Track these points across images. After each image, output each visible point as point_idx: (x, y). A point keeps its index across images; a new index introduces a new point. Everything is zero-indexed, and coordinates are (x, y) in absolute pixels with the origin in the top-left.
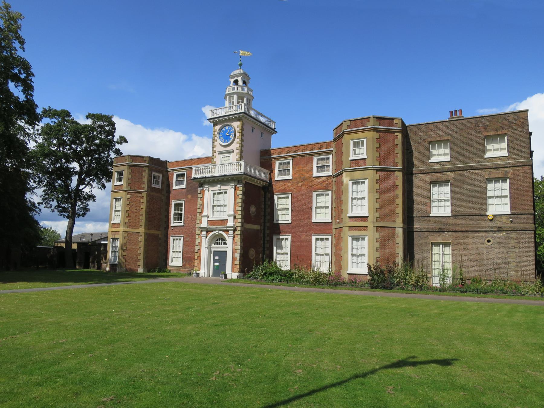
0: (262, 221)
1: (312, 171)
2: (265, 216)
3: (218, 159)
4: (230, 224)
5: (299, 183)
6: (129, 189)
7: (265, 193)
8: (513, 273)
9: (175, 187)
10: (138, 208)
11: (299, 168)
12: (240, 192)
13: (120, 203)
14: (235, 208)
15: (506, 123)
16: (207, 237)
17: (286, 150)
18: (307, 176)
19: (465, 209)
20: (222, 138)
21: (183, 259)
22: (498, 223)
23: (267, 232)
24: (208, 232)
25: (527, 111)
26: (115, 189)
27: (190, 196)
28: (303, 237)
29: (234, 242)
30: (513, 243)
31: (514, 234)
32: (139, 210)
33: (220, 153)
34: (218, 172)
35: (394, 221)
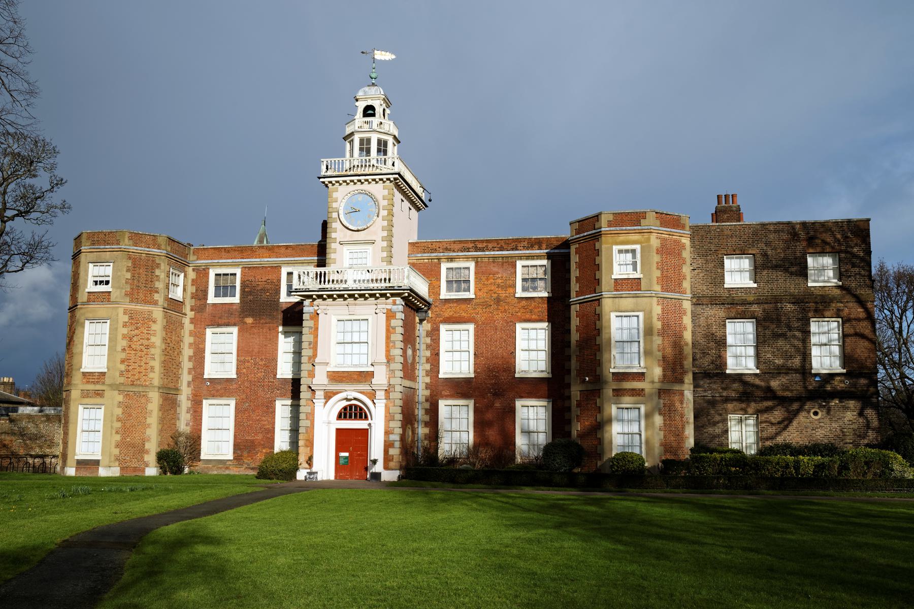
1: (514, 286)
4: (381, 378)
6: (166, 306)
9: (212, 299)
10: (145, 342)
11: (487, 279)
14: (388, 351)
17: (460, 246)
18: (503, 294)
21: (237, 446)
24: (328, 396)
25: (869, 220)
27: (249, 320)
32: (147, 347)
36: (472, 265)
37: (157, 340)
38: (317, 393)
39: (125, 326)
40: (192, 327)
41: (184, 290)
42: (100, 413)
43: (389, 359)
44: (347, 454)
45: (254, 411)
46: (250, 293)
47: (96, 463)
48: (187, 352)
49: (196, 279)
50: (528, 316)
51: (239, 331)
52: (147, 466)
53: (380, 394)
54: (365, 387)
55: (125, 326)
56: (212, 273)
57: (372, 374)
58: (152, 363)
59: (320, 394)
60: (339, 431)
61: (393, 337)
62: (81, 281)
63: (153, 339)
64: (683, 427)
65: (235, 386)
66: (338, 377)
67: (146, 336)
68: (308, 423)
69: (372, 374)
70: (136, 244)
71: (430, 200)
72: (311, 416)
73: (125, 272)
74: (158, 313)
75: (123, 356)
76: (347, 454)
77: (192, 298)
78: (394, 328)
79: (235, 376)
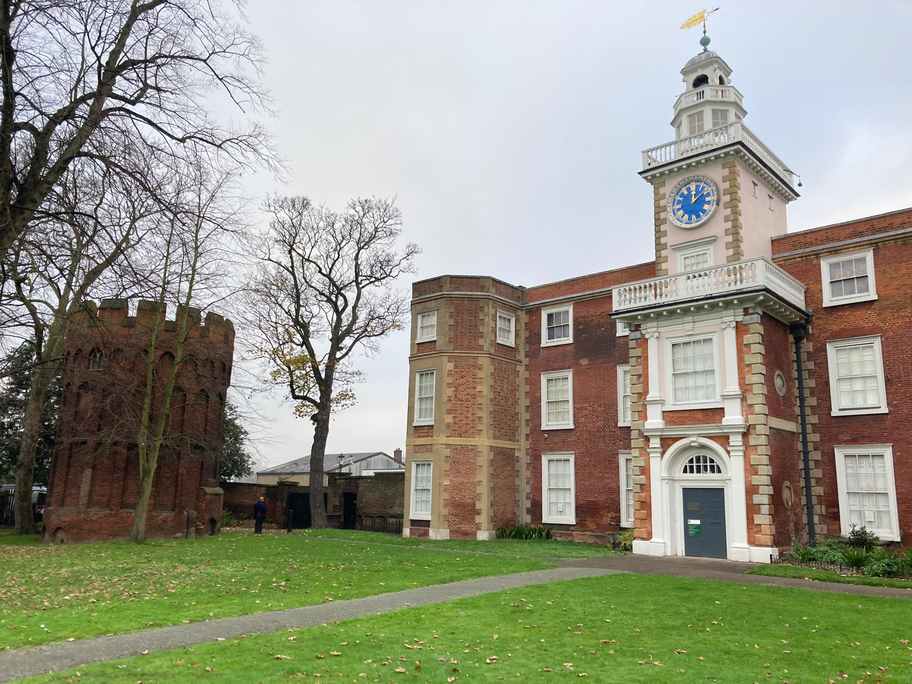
0: (797, 411)
2: (802, 399)
3: (676, 263)
4: (734, 417)
7: (798, 340)
9: (545, 342)
11: (897, 270)
12: (754, 338)
13: (432, 381)
14: (742, 378)
16: (663, 453)
21: (578, 508)
23: (814, 437)
24: (666, 442)
26: (419, 351)
27: (584, 362)
29: (751, 469)
32: (474, 397)
33: (677, 248)
34: (682, 290)
36: (869, 255)
38: (652, 441)
39: (450, 375)
40: (527, 374)
41: (517, 335)
43: (746, 389)
44: (698, 522)
45: (595, 466)
47: (427, 523)
48: (524, 402)
51: (574, 375)
52: (479, 529)
53: (736, 440)
55: (450, 375)
57: (719, 412)
58: (480, 414)
60: (688, 493)
61: (748, 359)
63: (479, 388)
65: (573, 438)
66: (672, 417)
67: (472, 385)
69: (719, 412)
70: (457, 289)
71: (800, 185)
73: (447, 319)
75: (449, 406)
76: (698, 522)
77: (526, 343)
78: (748, 346)
79: (572, 427)
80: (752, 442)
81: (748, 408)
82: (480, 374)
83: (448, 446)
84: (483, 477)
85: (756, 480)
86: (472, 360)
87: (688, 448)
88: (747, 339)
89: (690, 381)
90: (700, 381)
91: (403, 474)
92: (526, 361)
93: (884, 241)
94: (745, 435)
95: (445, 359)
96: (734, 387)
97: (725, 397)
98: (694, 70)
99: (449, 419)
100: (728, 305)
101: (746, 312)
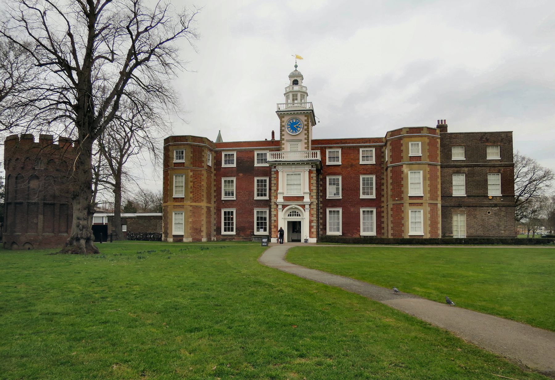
1: (359, 159)
4: (307, 199)
5: (348, 168)
8: (503, 232)
10: (200, 185)
12: (314, 175)
14: (310, 187)
15: (500, 139)
18: (354, 163)
19: (475, 192)
20: (290, 129)
22: (495, 202)
24: (284, 206)
27: (241, 175)
28: (352, 210)
29: (311, 215)
30: (503, 214)
31: (503, 209)
33: (288, 141)
35: (437, 200)
36: (340, 151)
37: (204, 183)
40: (215, 178)
42: (183, 217)
43: (310, 190)
46: (240, 163)
47: (182, 236)
49: (430, 142)
50: (365, 172)
53: (307, 207)
54: (300, 203)
56: (223, 154)
58: (203, 194)
59: (280, 207)
62: (413, 139)
63: (202, 183)
64: (437, 218)
66: (286, 198)
68: (275, 218)
72: (276, 216)
74: (204, 173)
75: (191, 190)
80: (312, 207)
81: (311, 197)
82: (203, 178)
83: (191, 206)
84: (204, 218)
85: (313, 219)
86: (199, 172)
87: (292, 208)
88: (312, 175)
89: (292, 187)
90: (295, 187)
91: (300, 222)
92: (215, 172)
93: (345, 147)
94: (310, 205)
95: (189, 171)
96: (308, 191)
97: (304, 193)
98: (294, 77)
99: (191, 195)
100: (308, 164)
101: (312, 167)
